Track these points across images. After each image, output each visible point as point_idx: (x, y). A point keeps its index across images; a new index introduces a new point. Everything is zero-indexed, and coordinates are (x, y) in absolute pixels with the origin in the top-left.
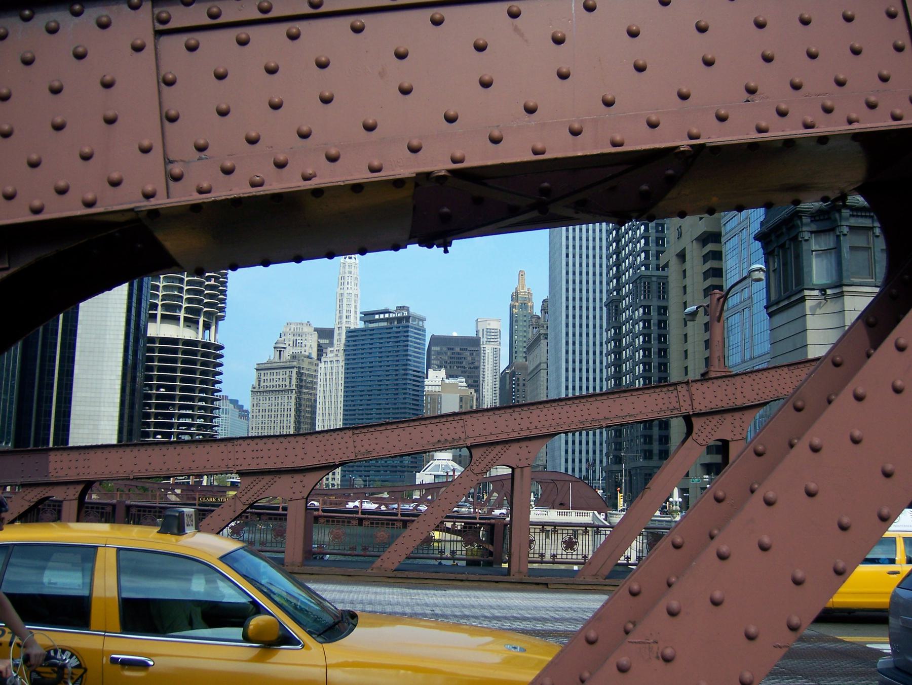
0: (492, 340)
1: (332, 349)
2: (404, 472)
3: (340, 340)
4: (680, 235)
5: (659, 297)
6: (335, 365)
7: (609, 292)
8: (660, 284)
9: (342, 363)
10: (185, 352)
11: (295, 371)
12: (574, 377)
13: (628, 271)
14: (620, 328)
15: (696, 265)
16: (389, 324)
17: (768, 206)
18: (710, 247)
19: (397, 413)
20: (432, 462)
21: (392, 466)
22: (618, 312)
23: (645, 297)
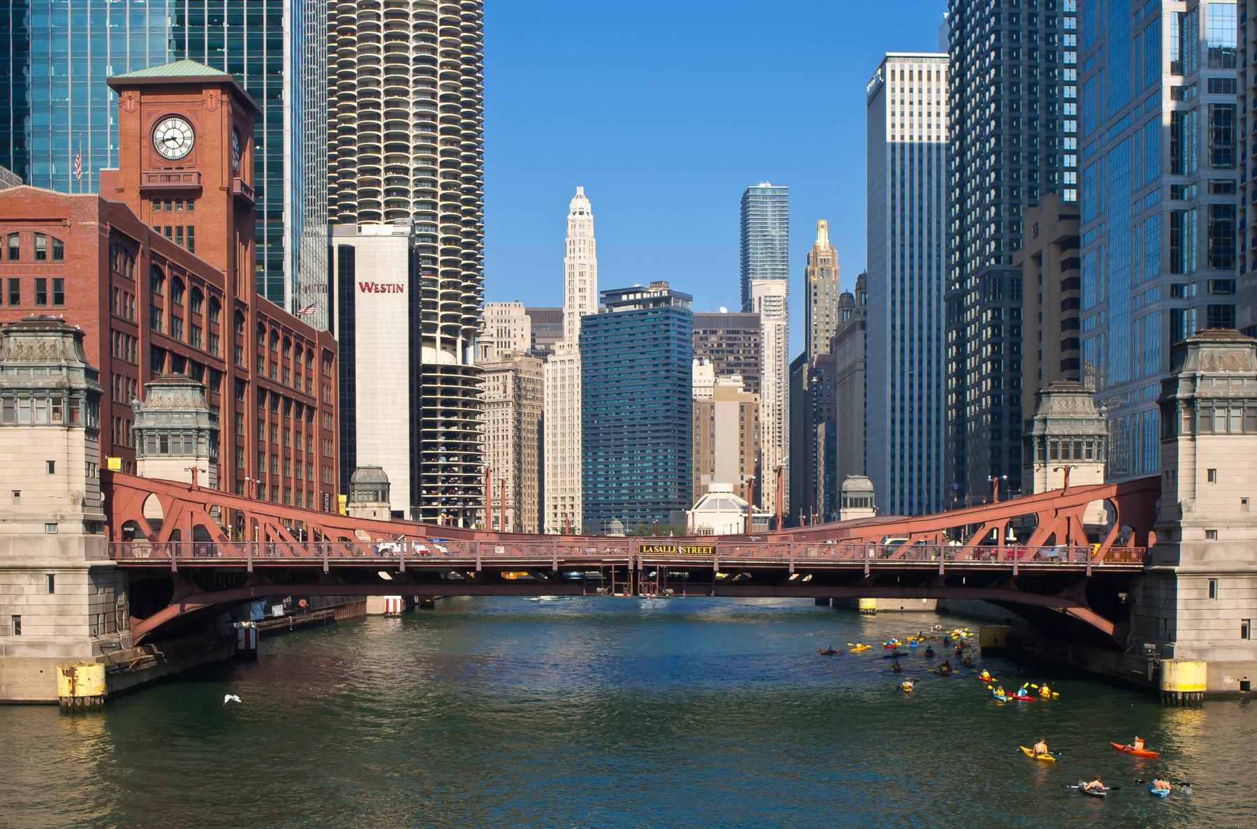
0: (772, 313)
1: (562, 344)
2: (669, 509)
3: (572, 328)
4: (1036, 233)
5: (1013, 298)
6: (567, 366)
7: (950, 283)
8: (1013, 280)
9: (578, 364)
10: (444, 381)
11: (510, 375)
12: (911, 407)
13: (974, 161)
14: (964, 330)
15: (1053, 274)
16: (642, 308)
17: (916, 681)
18: (1069, 253)
19: (658, 431)
20: (705, 495)
21: (653, 503)
22: (962, 310)
23: (994, 297)
